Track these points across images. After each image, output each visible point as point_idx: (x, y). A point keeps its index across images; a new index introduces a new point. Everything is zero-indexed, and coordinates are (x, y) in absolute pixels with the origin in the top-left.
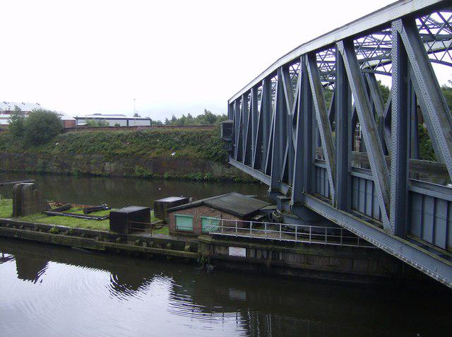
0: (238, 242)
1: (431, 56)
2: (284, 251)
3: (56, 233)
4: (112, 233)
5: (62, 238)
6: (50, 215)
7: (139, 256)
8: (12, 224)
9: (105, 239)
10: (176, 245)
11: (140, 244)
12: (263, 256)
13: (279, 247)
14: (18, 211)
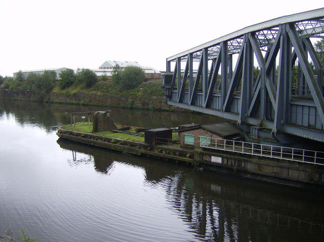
0: (217, 153)
1: (261, 48)
2: (244, 161)
3: (115, 143)
4: (146, 144)
5: (117, 146)
6: (114, 132)
7: (161, 160)
8: (91, 137)
9: (142, 148)
10: (182, 154)
11: (161, 152)
12: (232, 164)
13: (242, 158)
14: (96, 130)
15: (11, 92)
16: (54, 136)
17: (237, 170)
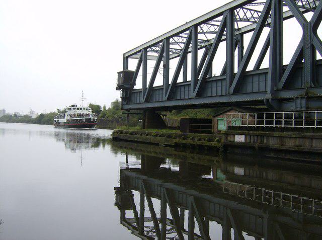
11: (193, 139)
15: (107, 120)
16: (118, 185)
17: (259, 147)
